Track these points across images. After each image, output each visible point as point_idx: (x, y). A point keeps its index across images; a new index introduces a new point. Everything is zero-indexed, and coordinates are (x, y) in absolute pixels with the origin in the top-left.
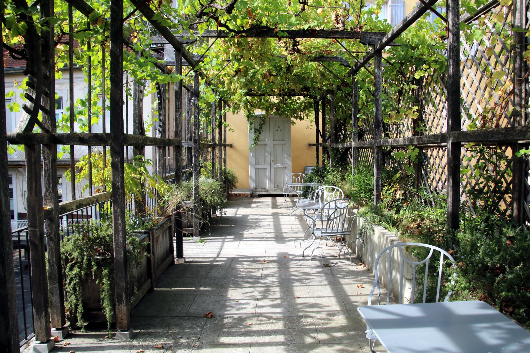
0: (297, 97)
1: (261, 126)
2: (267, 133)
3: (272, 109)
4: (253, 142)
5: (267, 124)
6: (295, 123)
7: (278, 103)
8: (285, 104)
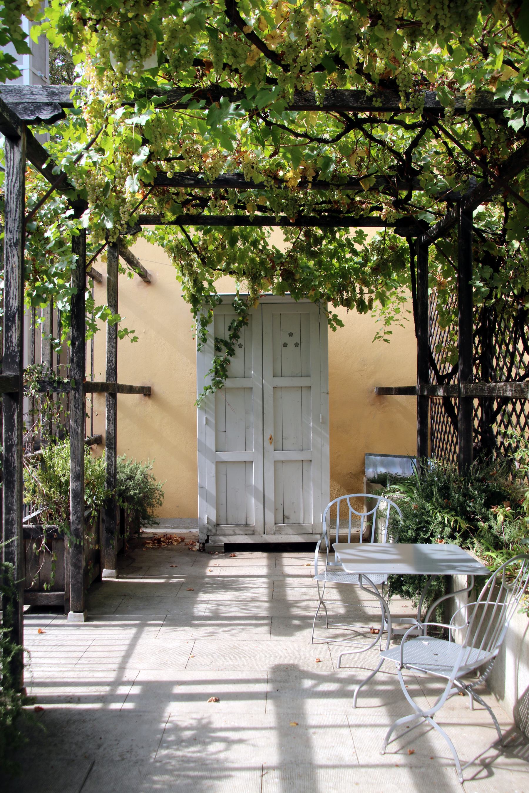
0: (353, 230)
1: (236, 329)
2: (255, 352)
3: (270, 276)
4: (209, 382)
5: (255, 324)
6: (340, 323)
8: (312, 255)
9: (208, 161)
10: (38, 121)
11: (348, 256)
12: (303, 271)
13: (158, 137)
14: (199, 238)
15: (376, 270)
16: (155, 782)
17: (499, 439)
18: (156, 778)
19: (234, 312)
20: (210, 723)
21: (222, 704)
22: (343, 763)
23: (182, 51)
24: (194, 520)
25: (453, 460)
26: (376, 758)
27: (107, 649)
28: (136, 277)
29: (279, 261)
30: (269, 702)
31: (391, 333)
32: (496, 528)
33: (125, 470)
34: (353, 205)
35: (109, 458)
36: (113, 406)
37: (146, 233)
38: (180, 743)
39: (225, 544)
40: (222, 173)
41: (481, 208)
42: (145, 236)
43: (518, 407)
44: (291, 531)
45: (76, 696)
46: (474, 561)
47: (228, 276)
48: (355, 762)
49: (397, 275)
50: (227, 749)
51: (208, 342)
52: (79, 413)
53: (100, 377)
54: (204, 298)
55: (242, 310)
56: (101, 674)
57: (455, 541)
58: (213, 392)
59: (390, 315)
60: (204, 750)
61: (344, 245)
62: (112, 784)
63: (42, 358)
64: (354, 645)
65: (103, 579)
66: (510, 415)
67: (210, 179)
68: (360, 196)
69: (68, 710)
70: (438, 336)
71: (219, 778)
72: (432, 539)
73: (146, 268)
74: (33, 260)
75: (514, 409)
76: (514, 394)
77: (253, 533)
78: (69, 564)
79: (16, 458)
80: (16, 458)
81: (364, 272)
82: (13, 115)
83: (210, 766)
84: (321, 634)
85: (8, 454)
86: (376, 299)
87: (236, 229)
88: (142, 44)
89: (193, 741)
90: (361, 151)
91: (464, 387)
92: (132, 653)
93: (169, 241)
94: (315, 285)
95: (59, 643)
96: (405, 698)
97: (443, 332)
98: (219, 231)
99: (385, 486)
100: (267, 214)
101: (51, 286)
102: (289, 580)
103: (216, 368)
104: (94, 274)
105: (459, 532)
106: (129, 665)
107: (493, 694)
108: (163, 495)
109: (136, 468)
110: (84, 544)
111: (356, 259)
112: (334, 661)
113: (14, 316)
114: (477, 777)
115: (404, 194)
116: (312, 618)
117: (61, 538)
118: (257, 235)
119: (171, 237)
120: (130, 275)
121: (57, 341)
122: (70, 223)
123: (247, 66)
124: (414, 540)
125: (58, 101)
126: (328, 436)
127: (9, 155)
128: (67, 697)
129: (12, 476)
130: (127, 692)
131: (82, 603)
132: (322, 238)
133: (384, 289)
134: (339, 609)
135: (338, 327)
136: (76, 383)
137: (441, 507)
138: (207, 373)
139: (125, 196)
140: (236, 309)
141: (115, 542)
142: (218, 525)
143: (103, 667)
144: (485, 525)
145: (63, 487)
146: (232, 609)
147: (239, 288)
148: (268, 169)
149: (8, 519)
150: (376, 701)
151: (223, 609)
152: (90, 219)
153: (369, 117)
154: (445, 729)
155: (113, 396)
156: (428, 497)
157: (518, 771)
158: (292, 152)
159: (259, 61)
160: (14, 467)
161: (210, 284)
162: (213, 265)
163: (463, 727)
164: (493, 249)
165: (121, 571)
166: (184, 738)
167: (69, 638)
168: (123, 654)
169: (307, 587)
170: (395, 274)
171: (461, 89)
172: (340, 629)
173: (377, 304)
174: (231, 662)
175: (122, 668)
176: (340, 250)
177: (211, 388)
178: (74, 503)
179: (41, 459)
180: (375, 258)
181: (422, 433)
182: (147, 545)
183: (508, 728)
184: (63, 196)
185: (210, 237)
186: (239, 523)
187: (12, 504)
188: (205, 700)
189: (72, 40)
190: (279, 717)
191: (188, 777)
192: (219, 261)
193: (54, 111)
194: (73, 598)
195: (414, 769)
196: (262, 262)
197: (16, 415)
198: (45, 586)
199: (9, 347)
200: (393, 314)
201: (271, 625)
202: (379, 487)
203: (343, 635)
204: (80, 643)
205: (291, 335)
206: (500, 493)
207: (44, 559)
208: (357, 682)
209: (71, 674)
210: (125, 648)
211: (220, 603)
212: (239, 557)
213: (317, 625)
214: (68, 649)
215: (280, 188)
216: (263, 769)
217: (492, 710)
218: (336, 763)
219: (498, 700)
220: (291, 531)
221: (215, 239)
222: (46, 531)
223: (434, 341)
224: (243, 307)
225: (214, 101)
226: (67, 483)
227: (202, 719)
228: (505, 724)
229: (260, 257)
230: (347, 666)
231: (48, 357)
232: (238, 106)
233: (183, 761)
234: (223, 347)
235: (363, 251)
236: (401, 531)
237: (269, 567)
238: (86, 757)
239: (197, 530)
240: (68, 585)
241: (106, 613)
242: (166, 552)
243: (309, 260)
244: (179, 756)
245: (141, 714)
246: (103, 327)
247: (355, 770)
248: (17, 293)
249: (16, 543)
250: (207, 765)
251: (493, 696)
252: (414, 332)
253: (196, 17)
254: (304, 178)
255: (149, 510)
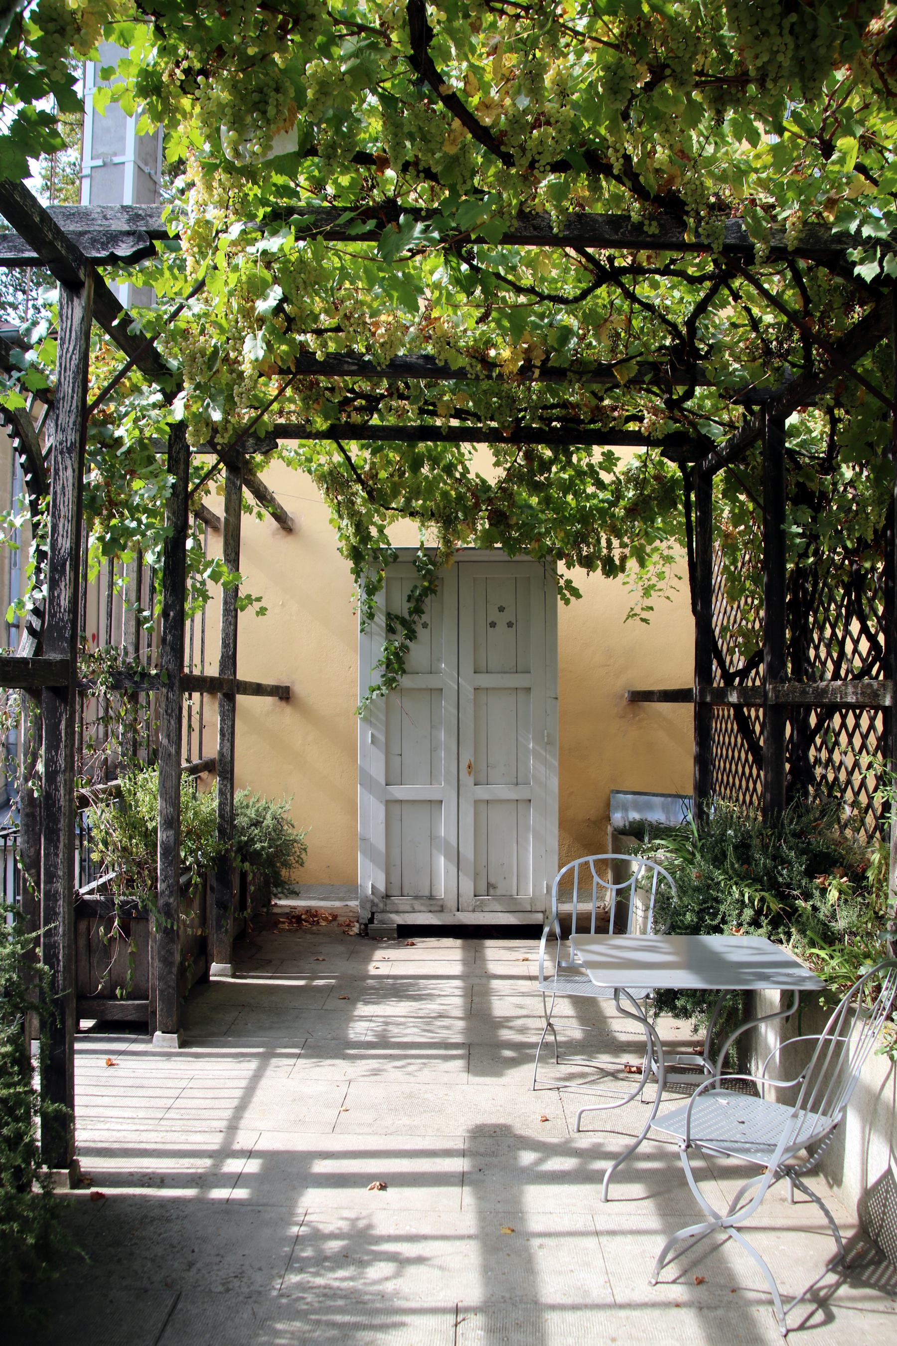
0: (598, 451)
1: (419, 600)
2: (447, 634)
4: (377, 678)
6: (576, 593)
7: (504, 490)
8: (536, 488)
9: (379, 332)
10: (113, 260)
11: (590, 489)
12: (522, 513)
13: (301, 286)
14: (365, 461)
15: (632, 511)
16: (278, 1333)
17: (819, 771)
18: (279, 1326)
19: (416, 575)
20: (370, 1226)
21: (392, 1192)
22: (589, 1301)
23: (338, 131)
24: (351, 888)
25: (751, 803)
26: (643, 1292)
27: (210, 1093)
28: (269, 521)
29: (484, 497)
30: (467, 1189)
31: (651, 608)
32: (824, 910)
33: (248, 812)
34: (598, 413)
35: (222, 793)
36: (229, 714)
37: (285, 453)
38: (322, 1262)
39: (399, 926)
40: (400, 353)
41: (793, 419)
42: (283, 458)
43: (850, 721)
44: (499, 908)
45: (158, 1174)
46: (795, 965)
47: (408, 520)
48: (609, 1300)
49: (663, 521)
50: (397, 1275)
51: (376, 618)
52: (173, 722)
53: (213, 670)
54: (370, 552)
55: (429, 571)
56: (198, 1138)
57: (760, 931)
58: (382, 695)
59: (651, 583)
60: (361, 1276)
61: (585, 473)
62: (208, 1336)
63: (124, 640)
64: (599, 1093)
65: (212, 978)
66: (838, 735)
67: (382, 360)
68: (611, 398)
69: (144, 1197)
70: (721, 615)
71: (384, 1327)
72: (725, 927)
73: (285, 509)
74: (107, 484)
75: (843, 725)
76: (861, 699)
77: (442, 909)
78: (156, 958)
79: (62, 792)
80: (62, 792)
81: (613, 515)
82: (72, 248)
83: (369, 1306)
84: (548, 1073)
85: (50, 786)
86: (632, 556)
87: (421, 447)
88: (270, 101)
89: (344, 1259)
90: (618, 322)
91: (774, 688)
92: (250, 1102)
93: (320, 465)
94: (540, 534)
95: (138, 1082)
96: (686, 1184)
97: (729, 608)
98: (396, 450)
99: (641, 839)
100: (469, 424)
101: (134, 524)
102: (495, 984)
103: (388, 659)
104: (208, 516)
105: (766, 916)
106: (243, 1123)
107: (822, 1175)
108: (305, 850)
109: (265, 809)
110: (178, 927)
111: (601, 495)
112: (569, 1120)
113: (64, 564)
114: (808, 1324)
115: (680, 390)
116: (533, 1046)
117: (143, 917)
118: (453, 456)
119: (323, 459)
120: (260, 515)
121: (146, 613)
122: (154, 413)
123: (446, 155)
124: (695, 930)
125: (144, 229)
126: (556, 764)
127: (65, 311)
128: (145, 1175)
129: (56, 821)
130: (238, 1170)
131: (175, 1018)
132: (552, 462)
133: (642, 541)
134: (572, 1030)
135: (573, 599)
136: (169, 676)
137: (738, 876)
138: (374, 666)
139: (243, 368)
140: (419, 569)
141: (229, 924)
142: (388, 896)
143: (204, 1125)
144: (808, 906)
145: (149, 836)
146: (409, 1031)
147: (423, 539)
148: (473, 347)
149: (50, 891)
150: (637, 1189)
151: (394, 1030)
152: (187, 407)
153: (632, 265)
154: (747, 1237)
155: (230, 698)
156: (718, 861)
157: (873, 1311)
158: (509, 317)
159: (464, 149)
160: (60, 808)
161: (381, 530)
162: (385, 501)
163: (779, 1234)
164: (812, 481)
165: (239, 966)
166: (328, 1253)
167: (153, 1075)
168: (235, 1103)
169: (523, 995)
170: (659, 520)
171: (780, 218)
172: (577, 1064)
173: (632, 564)
174: (405, 1121)
175: (232, 1128)
176: (577, 482)
177: (379, 689)
178: (163, 863)
179: (118, 793)
180: (631, 494)
181: (704, 760)
182: (281, 926)
183: (849, 1233)
184: (154, 385)
185: (381, 459)
186: (420, 894)
187: (56, 867)
188: (364, 1185)
189: (160, 108)
190: (483, 1216)
191: (334, 1325)
192: (395, 494)
193: (137, 243)
194: (161, 1010)
195: (705, 1310)
196: (460, 497)
197: (63, 723)
198: (118, 992)
199: (55, 613)
200: (654, 580)
201: (468, 1057)
202: (632, 842)
203: (583, 1075)
204: (170, 1083)
205: (501, 609)
206: (828, 855)
207: (117, 949)
208: (608, 1156)
209: (153, 1136)
210: (239, 1093)
211: (389, 1020)
212: (420, 945)
213: (543, 1059)
214: (151, 1093)
215: (489, 377)
216: (457, 1310)
217: (823, 1201)
218: (579, 1300)
219: (831, 1187)
220: (499, 908)
221: (389, 462)
222: (121, 907)
223: (717, 621)
224: (430, 566)
225: (389, 222)
226: (155, 829)
227: (357, 1219)
228: (847, 1227)
229: (456, 490)
230: (590, 1128)
231: (132, 638)
232: (428, 227)
233: (325, 1295)
234: (399, 627)
235: (613, 482)
236: (673, 914)
237: (465, 962)
238: (168, 1285)
239: (357, 903)
240: (154, 990)
241: (212, 1035)
242: (308, 936)
243: (531, 496)
244: (319, 1287)
245: (260, 1208)
246: (216, 591)
247: (608, 1312)
248: (68, 527)
249: (61, 930)
250: (364, 1303)
251: (821, 1178)
252: (690, 607)
253: (361, 64)
254: (528, 361)
255: (284, 873)
